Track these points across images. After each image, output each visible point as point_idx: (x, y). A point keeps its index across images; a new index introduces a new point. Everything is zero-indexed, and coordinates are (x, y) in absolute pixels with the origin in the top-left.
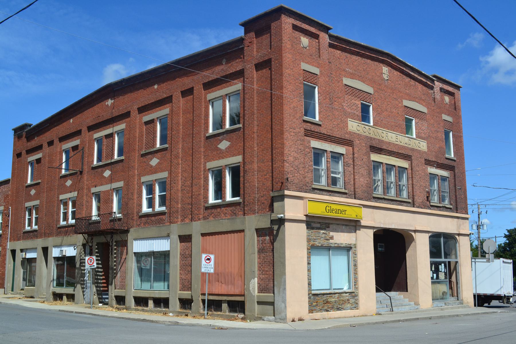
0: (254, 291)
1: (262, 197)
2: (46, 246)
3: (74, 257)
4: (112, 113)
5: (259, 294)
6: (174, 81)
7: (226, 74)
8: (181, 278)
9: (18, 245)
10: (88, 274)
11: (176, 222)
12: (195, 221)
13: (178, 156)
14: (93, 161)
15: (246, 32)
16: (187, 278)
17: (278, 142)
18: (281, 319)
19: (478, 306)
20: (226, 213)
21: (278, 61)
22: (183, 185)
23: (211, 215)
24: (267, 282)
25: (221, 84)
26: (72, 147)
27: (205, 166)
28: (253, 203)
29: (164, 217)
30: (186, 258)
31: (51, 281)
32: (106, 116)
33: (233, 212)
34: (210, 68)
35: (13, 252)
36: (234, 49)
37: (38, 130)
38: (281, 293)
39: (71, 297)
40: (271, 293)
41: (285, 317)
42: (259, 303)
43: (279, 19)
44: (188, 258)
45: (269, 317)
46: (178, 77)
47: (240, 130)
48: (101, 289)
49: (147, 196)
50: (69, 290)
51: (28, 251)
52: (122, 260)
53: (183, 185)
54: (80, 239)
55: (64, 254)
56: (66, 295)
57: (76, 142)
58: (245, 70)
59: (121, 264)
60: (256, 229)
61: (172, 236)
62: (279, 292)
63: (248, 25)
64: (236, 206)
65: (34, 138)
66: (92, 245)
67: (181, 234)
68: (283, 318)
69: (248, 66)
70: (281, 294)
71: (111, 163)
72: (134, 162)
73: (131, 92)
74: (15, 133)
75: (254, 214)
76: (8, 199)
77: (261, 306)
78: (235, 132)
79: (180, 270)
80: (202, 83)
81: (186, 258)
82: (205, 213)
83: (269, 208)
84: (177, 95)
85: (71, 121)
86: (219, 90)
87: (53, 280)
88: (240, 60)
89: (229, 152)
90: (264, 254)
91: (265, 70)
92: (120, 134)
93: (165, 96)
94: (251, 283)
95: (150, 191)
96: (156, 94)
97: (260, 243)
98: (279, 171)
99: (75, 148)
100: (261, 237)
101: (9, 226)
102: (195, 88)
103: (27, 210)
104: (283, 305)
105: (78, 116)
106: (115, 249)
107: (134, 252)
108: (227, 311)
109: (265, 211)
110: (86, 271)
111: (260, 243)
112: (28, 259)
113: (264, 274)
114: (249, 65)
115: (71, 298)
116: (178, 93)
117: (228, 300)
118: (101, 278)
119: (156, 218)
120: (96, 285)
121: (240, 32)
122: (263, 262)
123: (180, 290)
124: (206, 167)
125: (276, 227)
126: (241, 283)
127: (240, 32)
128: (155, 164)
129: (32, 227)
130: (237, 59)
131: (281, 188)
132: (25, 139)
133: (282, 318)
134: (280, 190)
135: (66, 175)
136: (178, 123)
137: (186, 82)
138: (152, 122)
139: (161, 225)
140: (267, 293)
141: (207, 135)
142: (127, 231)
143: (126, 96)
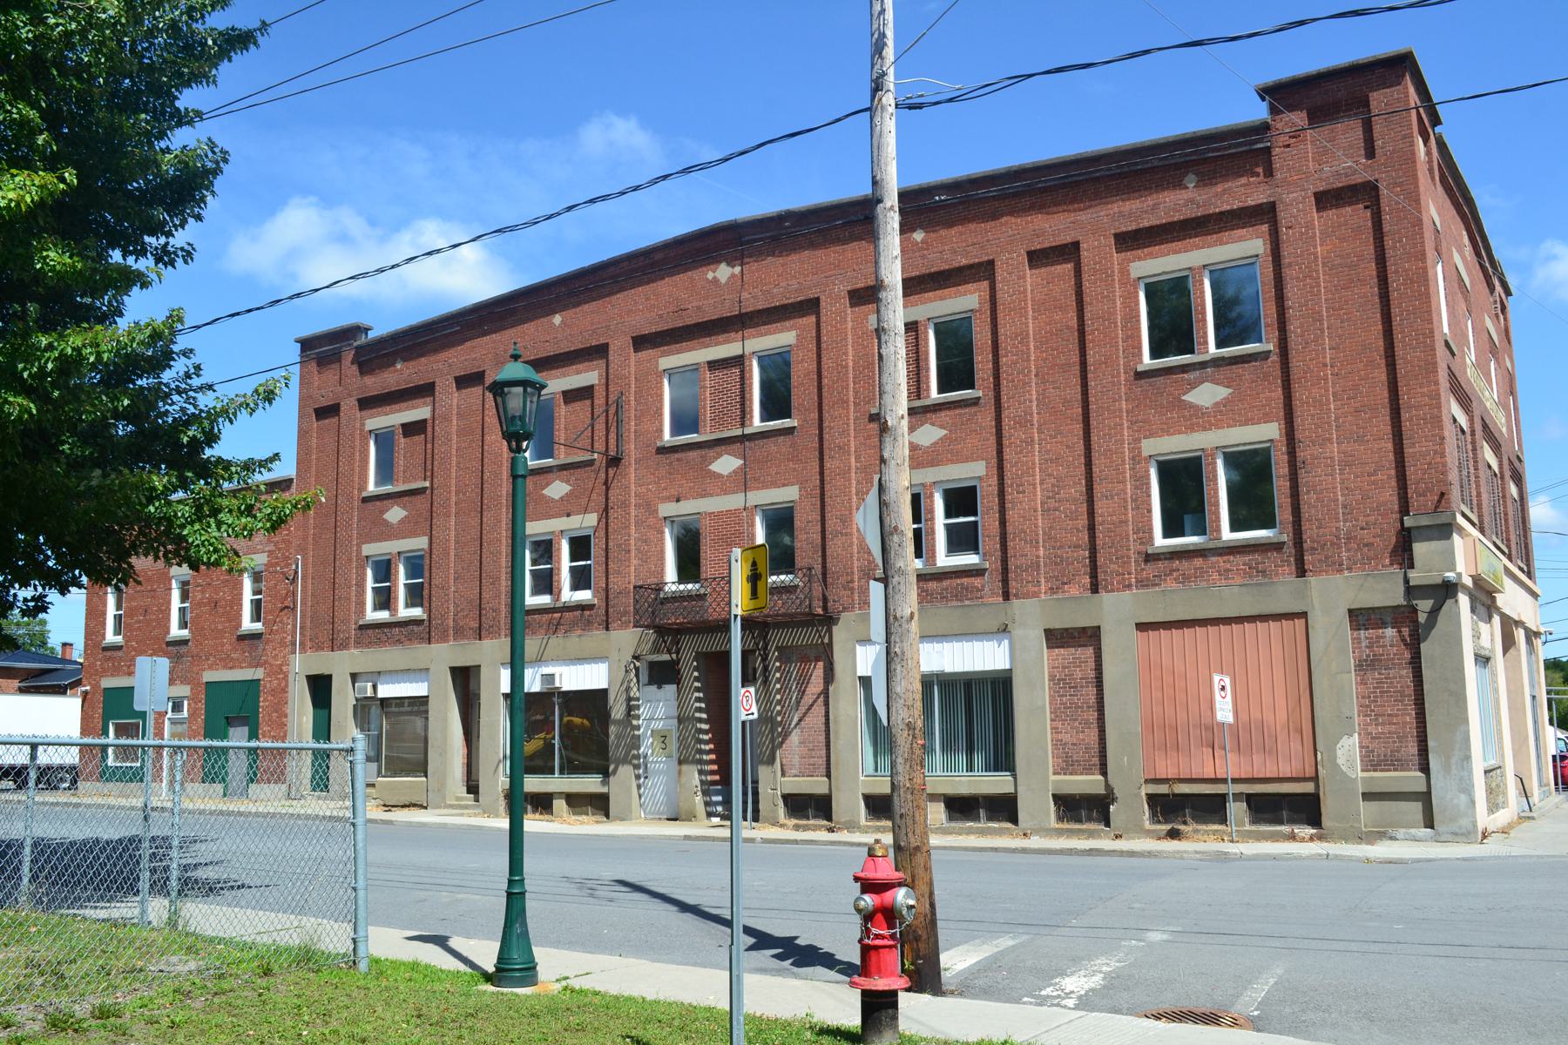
0: (1352, 767)
1: (1362, 529)
2: (327, 673)
3: (604, 692)
4: (740, 302)
5: (1366, 774)
6: (993, 223)
7: (1207, 212)
8: (1057, 743)
9: (338, 664)
10: (651, 740)
11: (1036, 595)
12: (1113, 591)
13: (1027, 421)
14: (660, 430)
15: (1274, 111)
16: (1083, 740)
17: (1419, 390)
18: (1456, 834)
19: (561, 772)
20: (1227, 570)
21: (1404, 188)
22: (1049, 498)
23: (1171, 574)
24: (1395, 742)
25: (1185, 239)
26: (403, 425)
27: (359, 551)
28: (1333, 544)
29: (977, 582)
30: (1076, 687)
31: (500, 761)
32: (712, 310)
33: (1257, 568)
34: (1136, 194)
35: (320, 687)
36: (1233, 151)
37: (411, 343)
38: (1454, 767)
39: (599, 804)
40: (1410, 770)
41: (1471, 827)
42: (1367, 796)
43: (1400, 84)
44: (1082, 687)
45: (1413, 831)
46: (1011, 214)
47: (1267, 358)
48: (709, 778)
49: (254, 595)
50: (589, 784)
51: (382, 678)
52: (805, 697)
53: (1049, 498)
54: (628, 639)
55: (557, 685)
56: (564, 796)
57: (418, 412)
58: (1280, 207)
59: (802, 709)
60: (1350, 611)
61: (1017, 632)
62: (1447, 768)
63: (1280, 94)
64: (1267, 551)
65: (393, 364)
66: (679, 660)
67: (1057, 626)
68: (1464, 830)
69: (1291, 195)
70: (1454, 771)
71: (744, 436)
72: (845, 433)
73: (813, 246)
74: (303, 350)
75: (1340, 571)
76: (287, 535)
77: (1375, 806)
78: (1249, 362)
79: (1052, 720)
80: (1113, 231)
81: (1076, 687)
82: (1143, 569)
83: (1391, 556)
84: (446, 386)
85: (557, 319)
86: (1175, 252)
87: (505, 757)
88: (1251, 179)
89: (565, 508)
90: (1379, 674)
91: (1349, 209)
92: (675, 378)
93: (964, 262)
94: (1339, 746)
95: (384, 570)
96: (923, 257)
97: (1363, 644)
98: (1430, 464)
99: (411, 429)
100: (1366, 629)
101: (294, 609)
102: (1083, 246)
103: (370, 563)
104: (1463, 797)
105: (586, 307)
106: (778, 669)
107: (859, 674)
108: (1247, 820)
109: (1377, 565)
110: (642, 730)
111: (1363, 644)
112: (383, 700)
113: (1383, 724)
114: (1294, 195)
115: (586, 806)
116: (1017, 256)
117: (1247, 794)
118: (707, 747)
119: (946, 583)
120: (699, 767)
121: (1258, 111)
122: (1375, 692)
123: (1054, 774)
124: (1140, 452)
125: (1425, 605)
126: (1300, 748)
127: (1258, 111)
128: (933, 441)
129: (394, 611)
130: (1242, 176)
131: (1436, 507)
132: (355, 368)
133: (1459, 832)
134: (1435, 512)
135: (542, 468)
136: (1025, 336)
137: (1052, 227)
138: (739, 361)
139: (967, 602)
140: (1395, 770)
141: (364, 494)
142: (829, 620)
143: (794, 257)
